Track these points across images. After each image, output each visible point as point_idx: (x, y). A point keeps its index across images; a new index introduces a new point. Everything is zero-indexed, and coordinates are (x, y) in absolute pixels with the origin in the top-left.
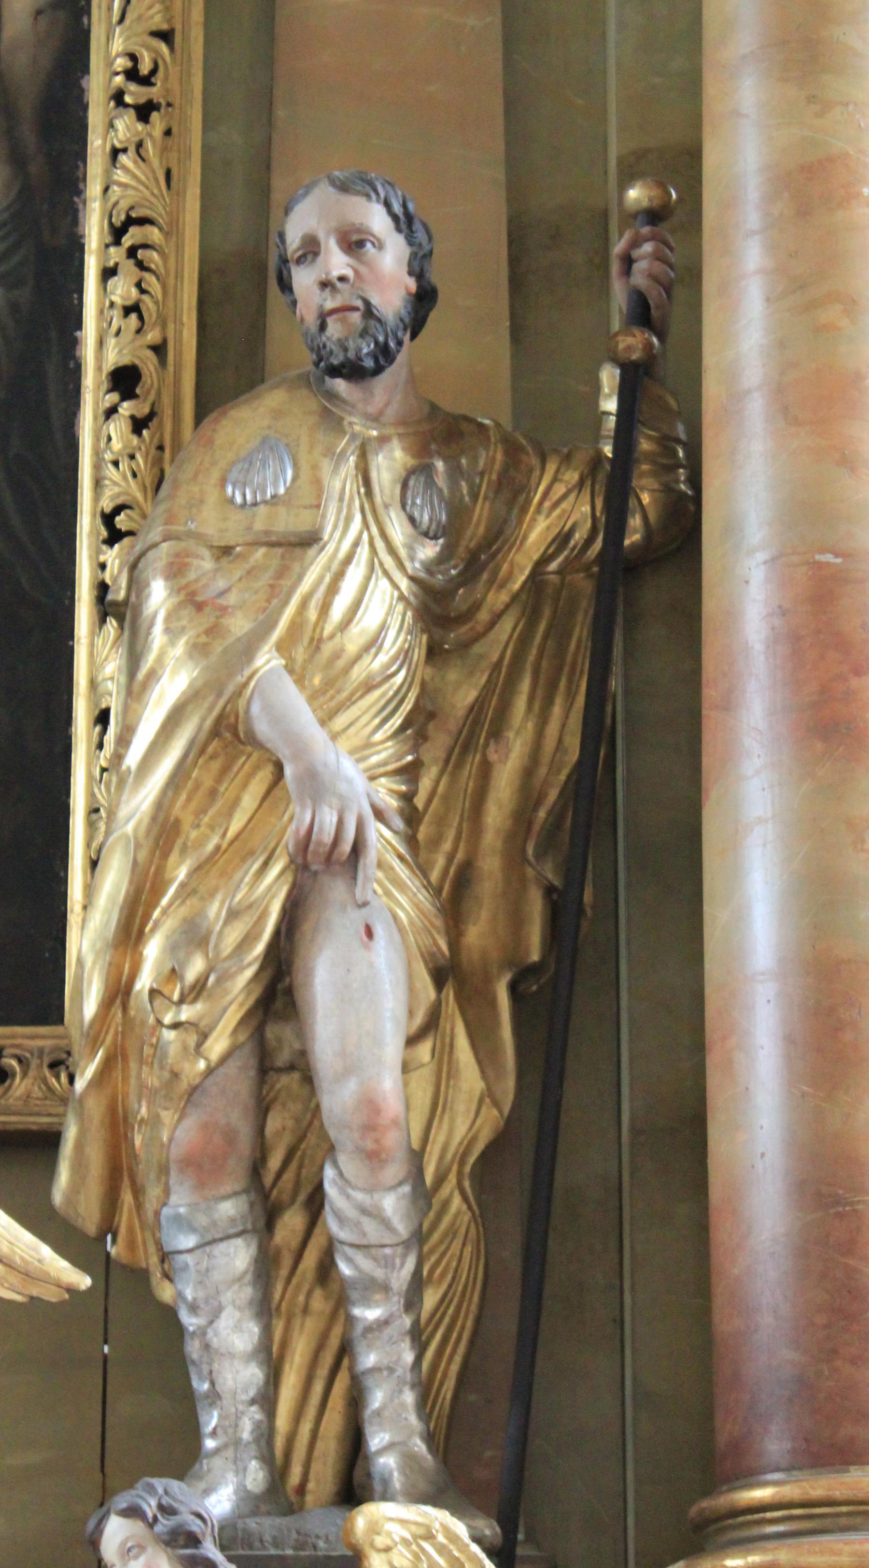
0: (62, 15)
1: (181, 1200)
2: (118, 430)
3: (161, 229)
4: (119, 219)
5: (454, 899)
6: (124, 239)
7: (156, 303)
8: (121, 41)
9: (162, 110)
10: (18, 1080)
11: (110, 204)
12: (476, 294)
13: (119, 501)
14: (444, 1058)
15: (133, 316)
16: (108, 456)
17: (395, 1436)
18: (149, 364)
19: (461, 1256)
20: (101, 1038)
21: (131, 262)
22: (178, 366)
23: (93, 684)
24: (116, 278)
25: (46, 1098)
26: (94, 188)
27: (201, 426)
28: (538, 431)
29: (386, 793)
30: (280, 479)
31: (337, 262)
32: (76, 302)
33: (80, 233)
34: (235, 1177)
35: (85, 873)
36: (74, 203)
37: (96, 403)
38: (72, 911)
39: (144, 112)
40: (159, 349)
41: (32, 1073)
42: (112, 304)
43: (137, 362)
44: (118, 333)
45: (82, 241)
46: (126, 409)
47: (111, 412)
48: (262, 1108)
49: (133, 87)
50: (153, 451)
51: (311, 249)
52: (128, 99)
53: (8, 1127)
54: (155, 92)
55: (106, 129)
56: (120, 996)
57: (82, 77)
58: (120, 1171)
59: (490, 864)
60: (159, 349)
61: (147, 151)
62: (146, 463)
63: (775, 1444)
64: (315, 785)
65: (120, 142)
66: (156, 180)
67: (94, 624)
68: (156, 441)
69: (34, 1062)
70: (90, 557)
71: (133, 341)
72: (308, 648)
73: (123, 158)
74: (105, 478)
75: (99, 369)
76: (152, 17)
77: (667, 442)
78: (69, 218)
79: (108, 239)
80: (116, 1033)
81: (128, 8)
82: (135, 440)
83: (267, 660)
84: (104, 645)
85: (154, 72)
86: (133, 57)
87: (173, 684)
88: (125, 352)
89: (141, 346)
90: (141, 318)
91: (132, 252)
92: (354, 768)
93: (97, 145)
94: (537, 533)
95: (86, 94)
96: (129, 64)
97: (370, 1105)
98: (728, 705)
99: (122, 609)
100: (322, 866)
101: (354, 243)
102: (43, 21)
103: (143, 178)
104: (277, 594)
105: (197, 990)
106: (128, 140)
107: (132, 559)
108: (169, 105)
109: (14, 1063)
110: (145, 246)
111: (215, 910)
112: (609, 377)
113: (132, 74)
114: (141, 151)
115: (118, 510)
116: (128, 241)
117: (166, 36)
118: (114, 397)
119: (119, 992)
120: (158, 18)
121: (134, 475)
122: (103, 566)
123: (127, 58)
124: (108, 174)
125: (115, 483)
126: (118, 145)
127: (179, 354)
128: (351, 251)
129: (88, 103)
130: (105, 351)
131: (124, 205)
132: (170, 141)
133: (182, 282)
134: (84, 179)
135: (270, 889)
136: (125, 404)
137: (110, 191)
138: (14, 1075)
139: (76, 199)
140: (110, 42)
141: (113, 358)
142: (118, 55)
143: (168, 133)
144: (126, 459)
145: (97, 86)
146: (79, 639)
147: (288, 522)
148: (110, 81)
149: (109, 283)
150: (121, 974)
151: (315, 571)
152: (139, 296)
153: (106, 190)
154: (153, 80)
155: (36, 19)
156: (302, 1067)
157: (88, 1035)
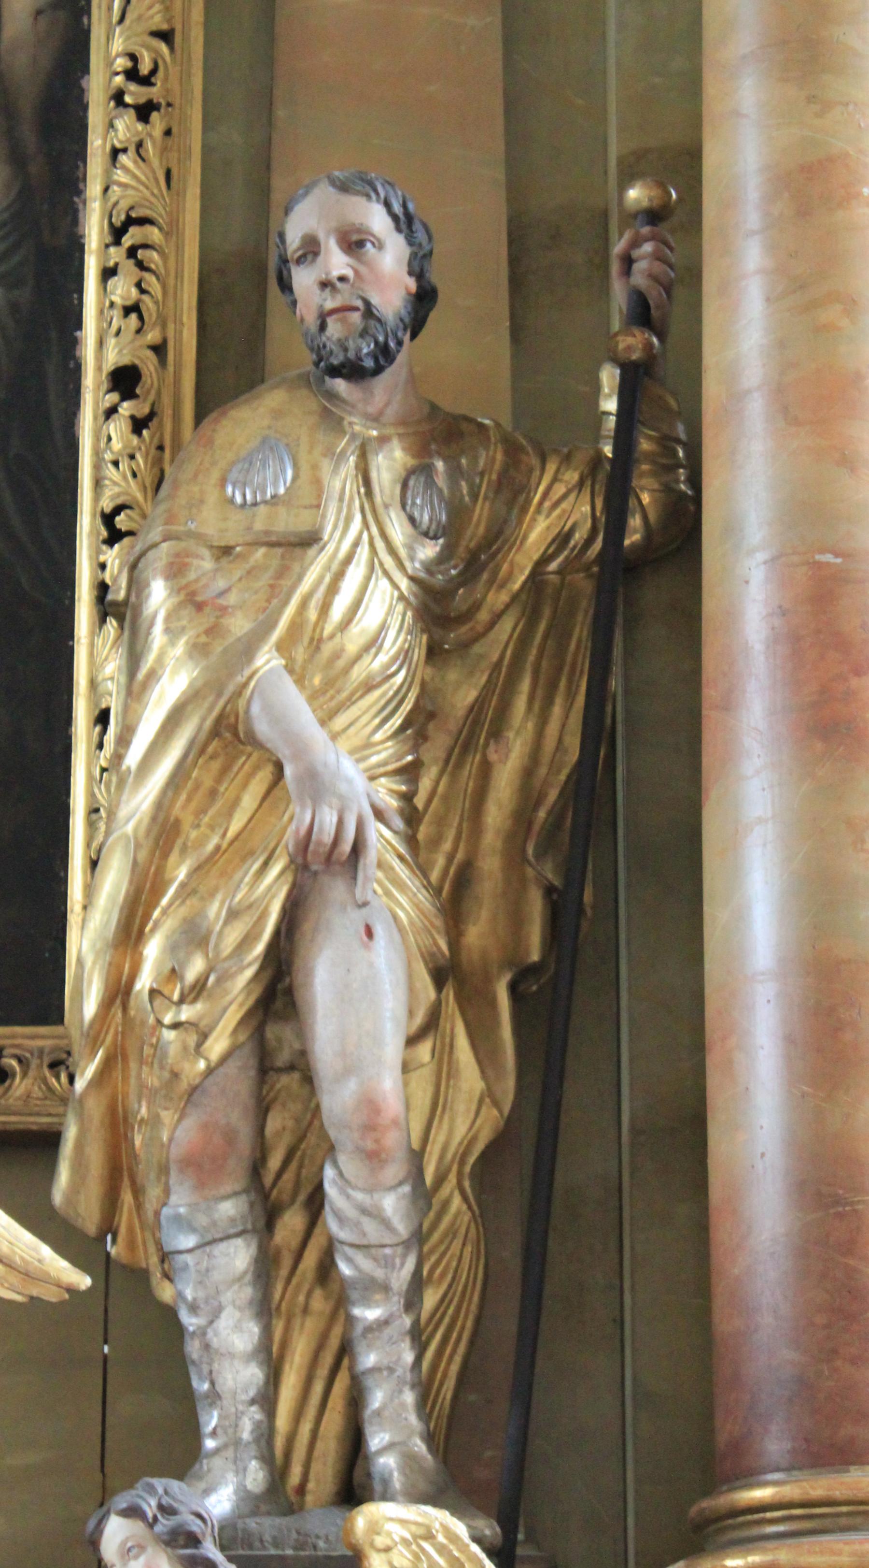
0: (62, 15)
1: (181, 1200)
2: (118, 430)
3: (161, 229)
4: (119, 219)
5: (454, 899)
6: (124, 239)
7: (156, 303)
8: (121, 41)
9: (162, 110)
10: (18, 1080)
11: (110, 204)
12: (476, 294)
13: (119, 501)
14: (444, 1058)
15: (133, 316)
16: (108, 456)
17: (395, 1436)
18: (149, 364)
19: (461, 1256)
20: (101, 1038)
21: (131, 262)
22: (178, 366)
23: (93, 684)
24: (116, 278)
25: (46, 1098)
26: (94, 188)
27: (201, 426)
28: (538, 431)
29: (386, 793)
30: (280, 479)
31: (337, 262)
32: (76, 302)
33: (80, 233)
34: (235, 1177)
35: (85, 873)
36: (74, 203)
37: (96, 403)
38: (72, 911)
39: (144, 112)
40: (159, 349)
41: (32, 1073)
42: (112, 304)
43: (137, 362)
44: (118, 333)
45: (82, 241)
46: (126, 409)
47: (111, 412)
48: (262, 1108)
49: (133, 87)
50: (153, 451)
51: (311, 249)
52: (128, 99)
53: (8, 1127)
54: (155, 92)
55: (106, 129)
56: (120, 996)
57: (82, 77)
58: (120, 1171)
59: (490, 864)
60: (159, 349)
61: (147, 151)
62: (146, 463)
63: (775, 1444)
64: (315, 785)
65: (120, 142)
66: (156, 180)
67: (94, 624)
68: (156, 441)
69: (34, 1062)
70: (90, 557)
71: (133, 341)
72: (308, 648)
73: (123, 158)
74: (105, 478)
75: (99, 369)
76: (152, 17)
77: (667, 442)
78: (69, 218)
79: (108, 239)
80: (116, 1033)
81: (128, 8)
82: (135, 440)
83: (267, 660)
84: (104, 645)
85: (154, 72)
86: (133, 57)
87: (173, 684)
88: (125, 352)
89: (141, 346)
90: (141, 318)
91: (132, 252)
92: (354, 768)
93: (97, 145)
94: (537, 533)
95: (86, 94)
96: (129, 64)
97: (370, 1105)
98: (728, 705)
99: (122, 609)
100: (322, 866)
101: (354, 243)
102: (43, 21)
103: (143, 178)
104: (277, 594)
105: (197, 990)
106: (128, 140)
107: (132, 559)
108: (169, 105)
109: (14, 1063)
110: (145, 246)
111: (215, 910)
112: (609, 377)
113: (132, 74)
114: (141, 151)
115: (118, 510)
116: (128, 241)
117: (166, 36)
118: (114, 397)
119: (119, 992)
120: (158, 18)
121: (134, 475)
122: (103, 566)
123: (127, 58)
124: (108, 174)
125: (115, 483)
126: (118, 145)
127: (179, 354)
128: (351, 251)
129: (88, 103)
130: (105, 351)
131: (124, 205)
132: (170, 141)
133: (182, 282)
134: (84, 179)
135: (270, 889)
136: (125, 404)
137: (110, 191)
138: (14, 1075)
139: (76, 199)
140: (110, 42)
141: (113, 358)
142: (118, 55)
143: (168, 133)
144: (126, 459)
145: (97, 86)
146: (79, 639)
147: (288, 522)
148: (110, 81)
149: (109, 283)
150: (121, 974)
151: (315, 571)
152: (139, 296)
153: (106, 190)
154: (153, 80)
155: (36, 19)
156: (302, 1067)
157: (88, 1035)
